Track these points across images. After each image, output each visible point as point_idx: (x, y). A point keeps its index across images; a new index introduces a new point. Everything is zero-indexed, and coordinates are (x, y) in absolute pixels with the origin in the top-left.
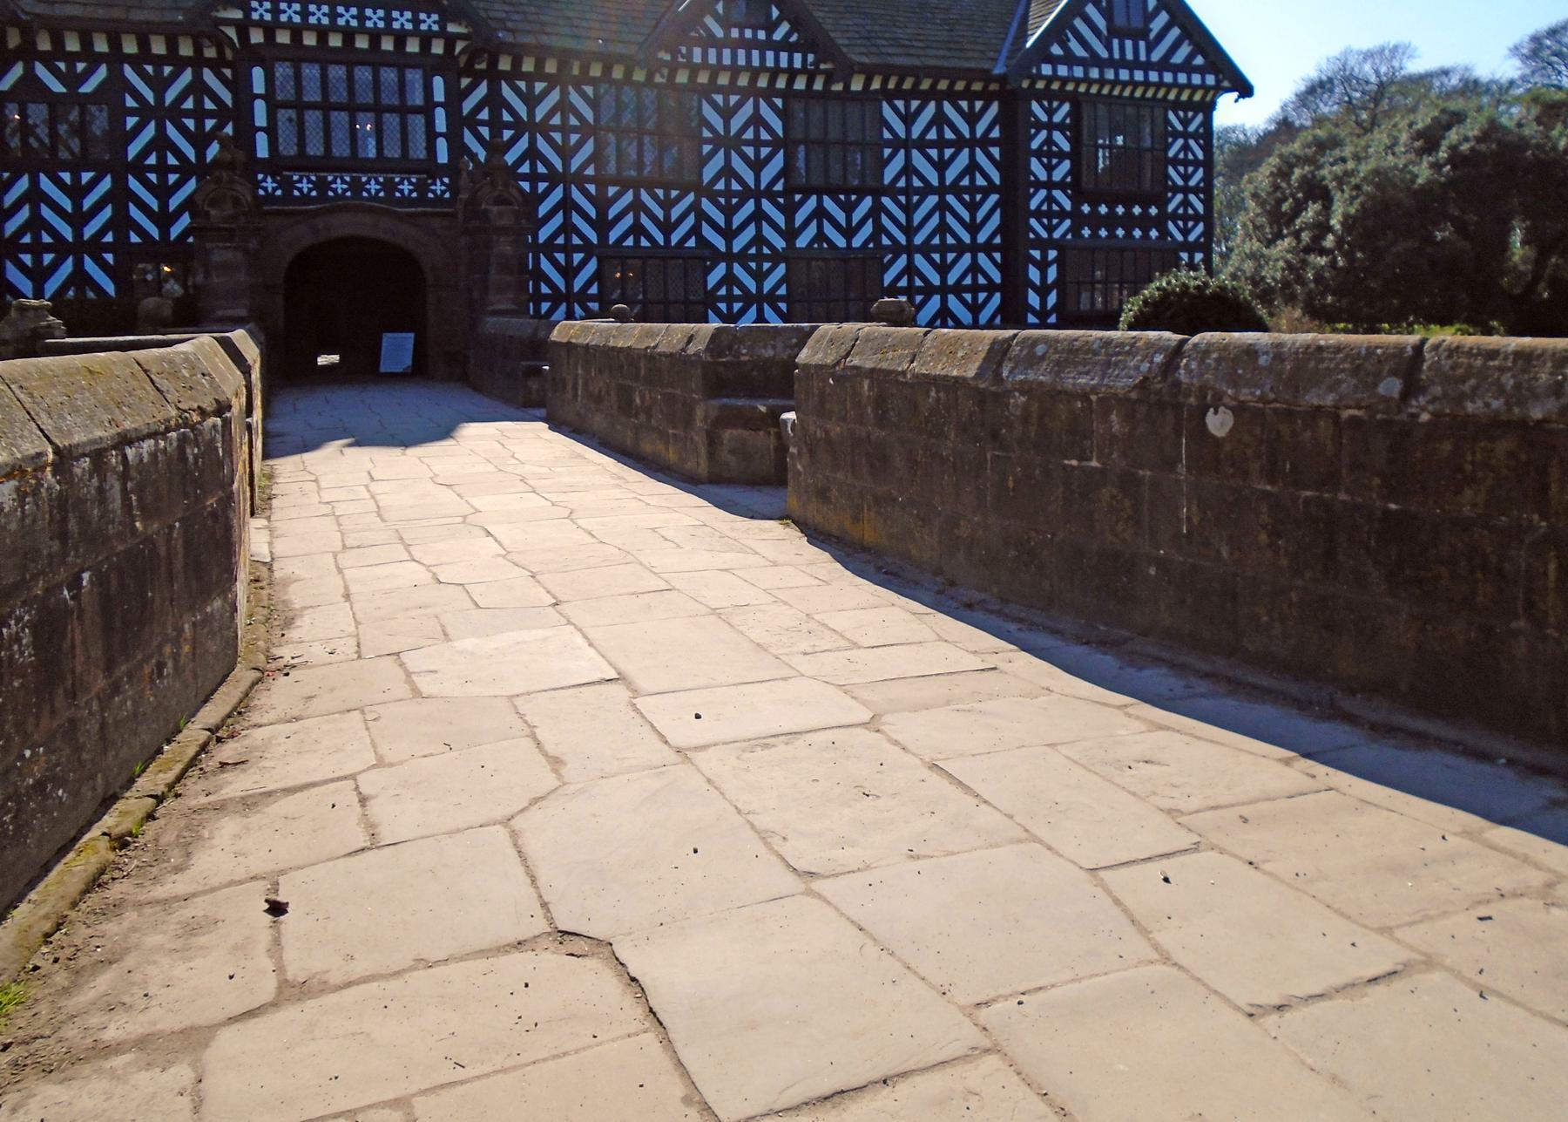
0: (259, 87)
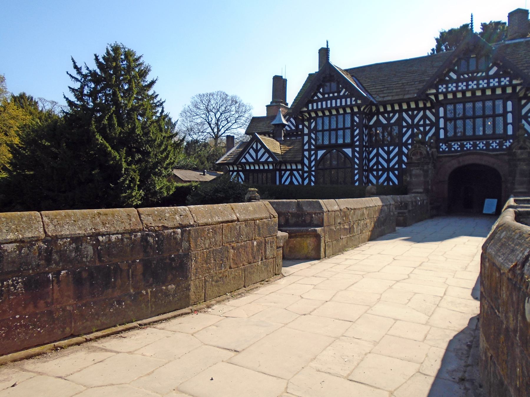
0: (442, 114)
